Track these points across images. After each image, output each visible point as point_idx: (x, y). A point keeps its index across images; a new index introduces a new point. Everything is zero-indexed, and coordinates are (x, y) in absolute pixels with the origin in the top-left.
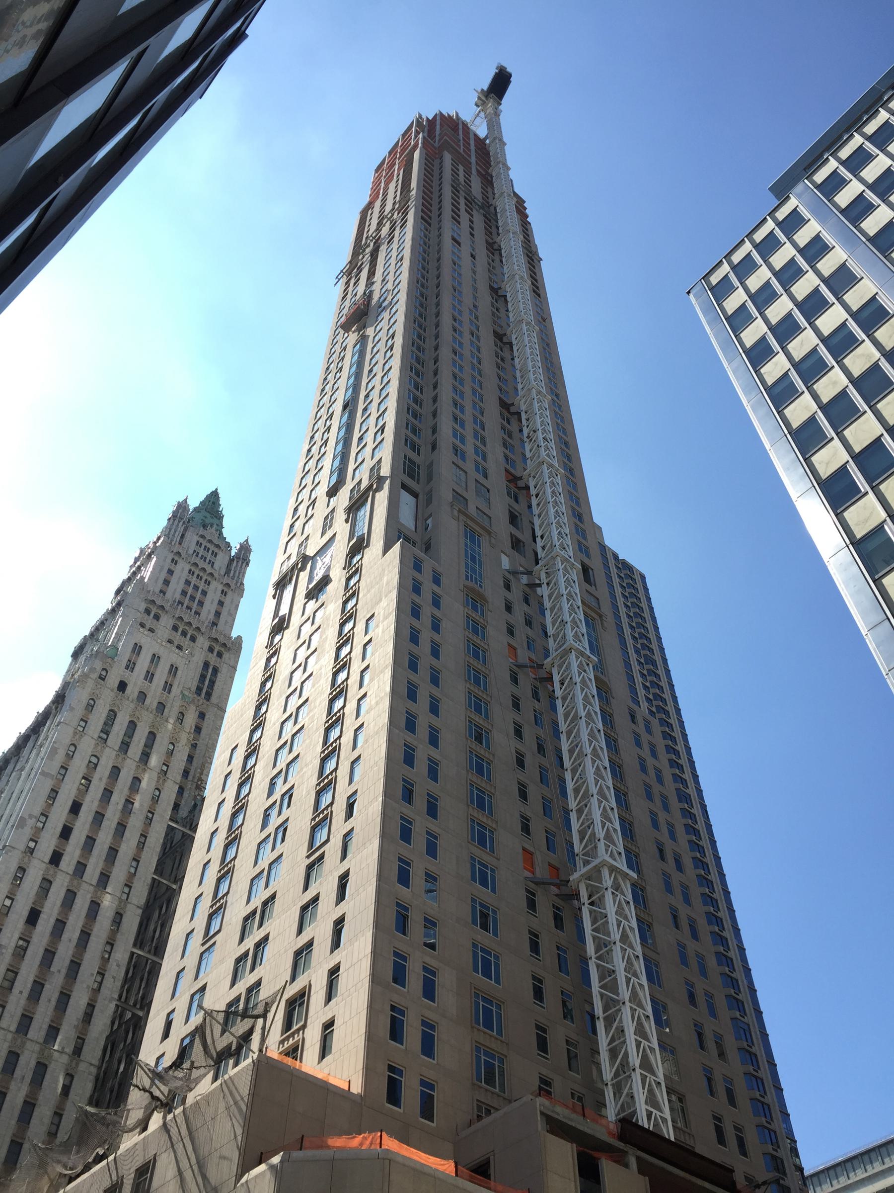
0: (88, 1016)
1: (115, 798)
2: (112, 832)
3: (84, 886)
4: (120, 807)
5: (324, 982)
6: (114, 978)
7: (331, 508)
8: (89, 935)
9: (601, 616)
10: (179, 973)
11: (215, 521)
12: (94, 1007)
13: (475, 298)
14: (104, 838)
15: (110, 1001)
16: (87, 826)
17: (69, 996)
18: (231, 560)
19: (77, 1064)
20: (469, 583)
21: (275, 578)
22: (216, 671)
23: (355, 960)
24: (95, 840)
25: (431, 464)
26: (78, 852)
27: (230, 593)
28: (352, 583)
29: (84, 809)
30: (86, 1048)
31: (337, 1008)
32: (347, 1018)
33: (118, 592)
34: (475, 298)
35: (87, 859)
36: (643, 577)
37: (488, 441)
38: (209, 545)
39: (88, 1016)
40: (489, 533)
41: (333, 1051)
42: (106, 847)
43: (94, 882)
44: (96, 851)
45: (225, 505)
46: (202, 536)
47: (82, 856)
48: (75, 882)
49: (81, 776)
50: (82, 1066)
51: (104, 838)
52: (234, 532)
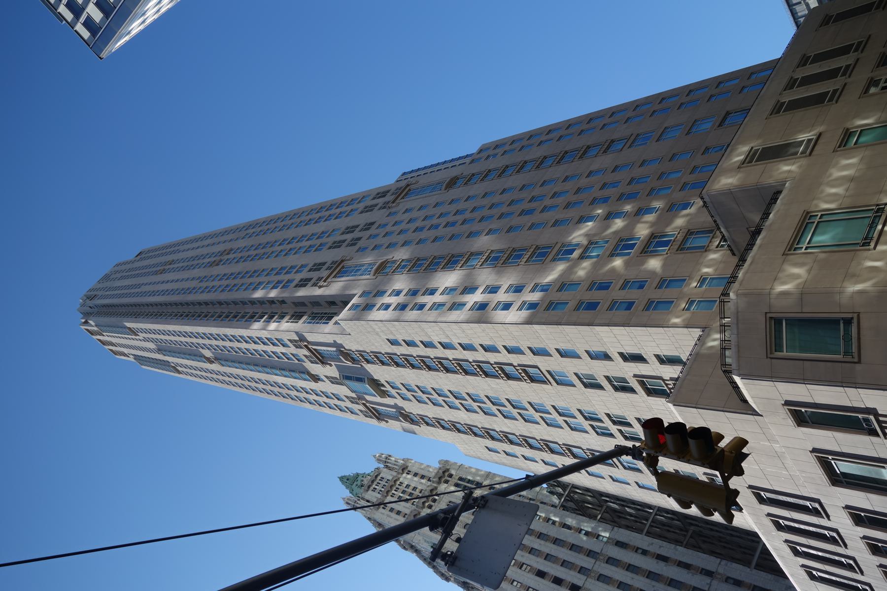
0: (687, 566)
1: (536, 546)
2: (559, 548)
3: (596, 568)
4: (542, 542)
5: (632, 364)
6: (660, 547)
7: (325, 379)
8: (630, 565)
9: (408, 185)
10: (640, 487)
11: (360, 478)
12: (680, 562)
13: (193, 279)
14: (564, 554)
15: (677, 550)
16: (554, 565)
17: (672, 579)
18: (387, 467)
19: (719, 574)
20: (372, 272)
21: (374, 422)
22: (461, 479)
23: (615, 340)
24: (564, 561)
25: (294, 303)
26: (572, 573)
27: (409, 469)
28: (462, 429)
29: (542, 568)
30: (708, 568)
31: (648, 354)
32: (654, 344)
33: (404, 548)
34: (193, 279)
35: (577, 566)
36: (404, 174)
37: (284, 265)
38: (375, 483)
39: (687, 566)
40: (342, 261)
41: (678, 354)
42: (570, 552)
43: (593, 561)
44: (572, 560)
45: (349, 472)
46: (369, 487)
47: (575, 570)
48: (592, 574)
49: (519, 570)
50: (721, 570)
51: (564, 554)
52: (368, 467)
